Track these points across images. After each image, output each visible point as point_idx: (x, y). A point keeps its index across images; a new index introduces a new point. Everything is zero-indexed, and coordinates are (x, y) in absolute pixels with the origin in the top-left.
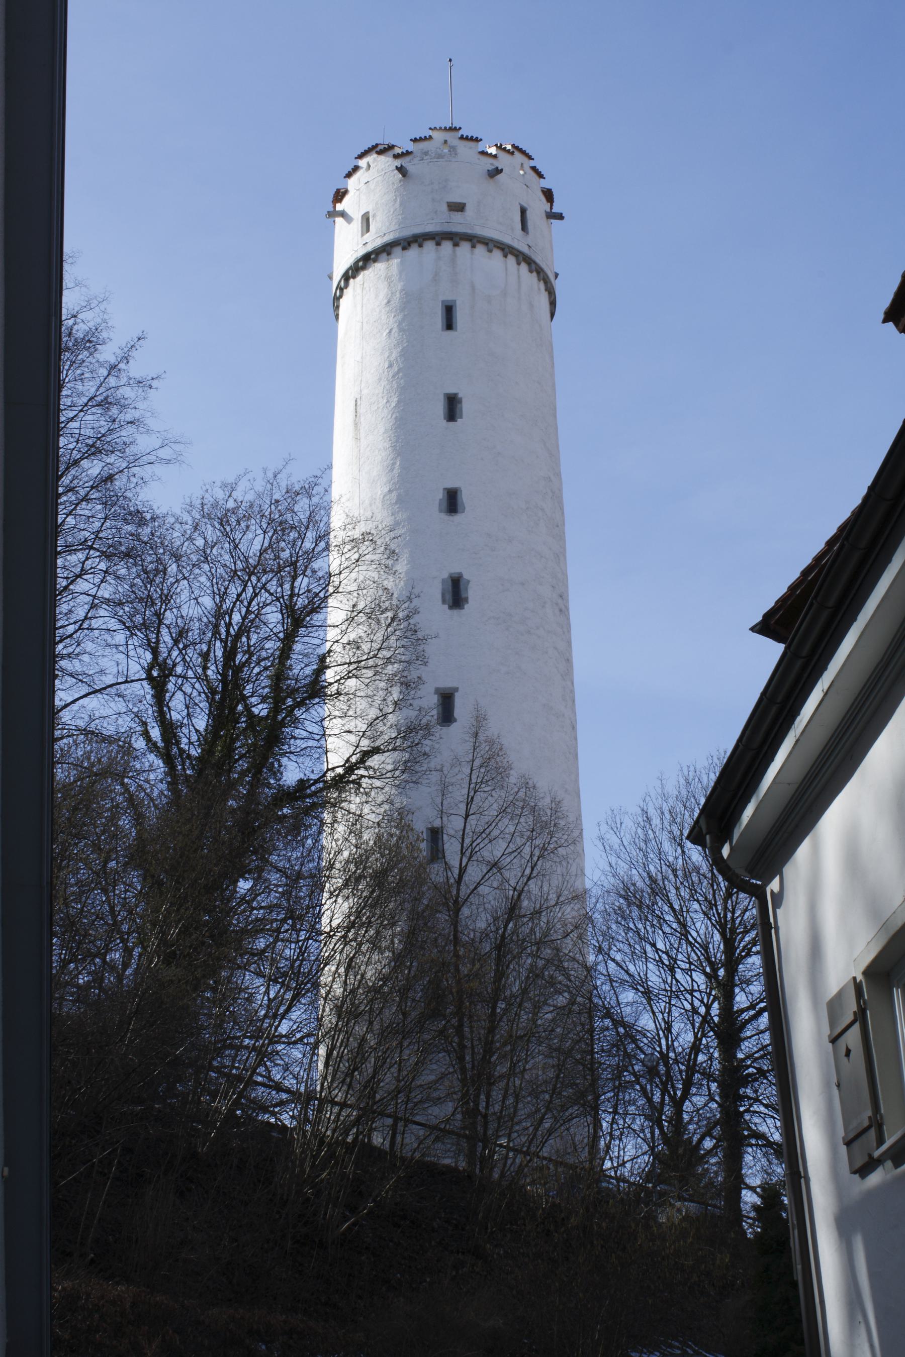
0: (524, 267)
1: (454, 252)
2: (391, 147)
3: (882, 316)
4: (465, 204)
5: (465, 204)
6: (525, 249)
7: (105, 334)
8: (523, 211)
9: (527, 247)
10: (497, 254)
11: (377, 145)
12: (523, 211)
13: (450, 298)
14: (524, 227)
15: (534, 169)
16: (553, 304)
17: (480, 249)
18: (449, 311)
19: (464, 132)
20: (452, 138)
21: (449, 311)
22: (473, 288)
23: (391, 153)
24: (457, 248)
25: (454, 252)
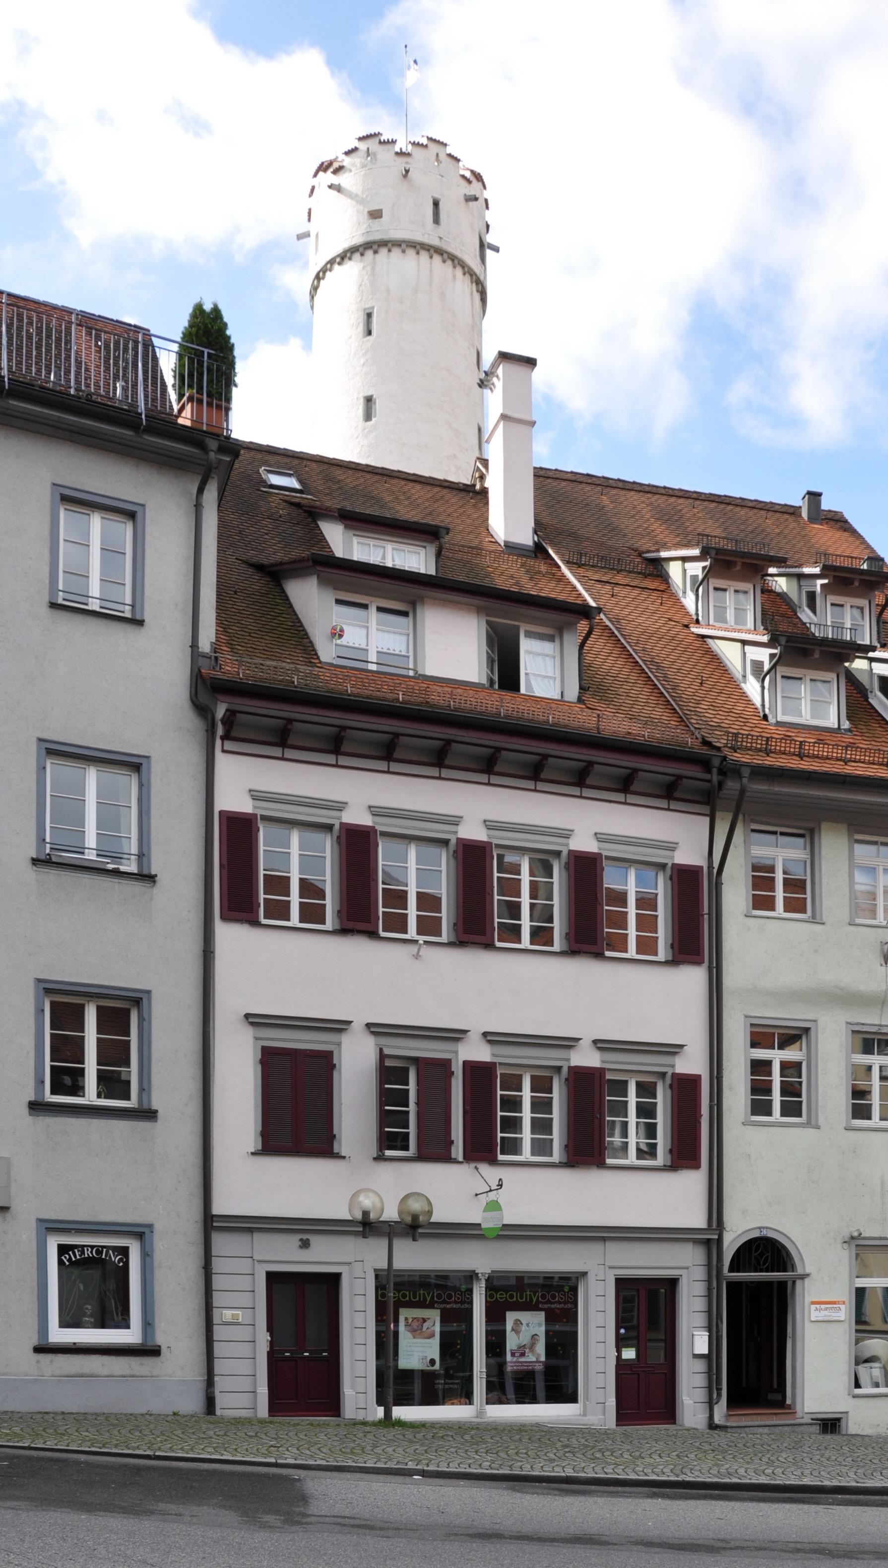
0: (437, 259)
1: (374, 259)
2: (330, 164)
3: (220, 307)
4: (381, 210)
5: (381, 210)
6: (435, 242)
7: (208, 307)
8: (436, 204)
9: (438, 240)
10: (411, 252)
11: (323, 163)
12: (436, 204)
13: (828, 1437)
14: (436, 220)
15: (450, 155)
16: (484, 300)
17: (396, 251)
18: (197, 126)
19: (384, 138)
20: (372, 144)
21: (197, 126)
22: (388, 291)
23: (331, 170)
24: (377, 256)
25: (374, 259)
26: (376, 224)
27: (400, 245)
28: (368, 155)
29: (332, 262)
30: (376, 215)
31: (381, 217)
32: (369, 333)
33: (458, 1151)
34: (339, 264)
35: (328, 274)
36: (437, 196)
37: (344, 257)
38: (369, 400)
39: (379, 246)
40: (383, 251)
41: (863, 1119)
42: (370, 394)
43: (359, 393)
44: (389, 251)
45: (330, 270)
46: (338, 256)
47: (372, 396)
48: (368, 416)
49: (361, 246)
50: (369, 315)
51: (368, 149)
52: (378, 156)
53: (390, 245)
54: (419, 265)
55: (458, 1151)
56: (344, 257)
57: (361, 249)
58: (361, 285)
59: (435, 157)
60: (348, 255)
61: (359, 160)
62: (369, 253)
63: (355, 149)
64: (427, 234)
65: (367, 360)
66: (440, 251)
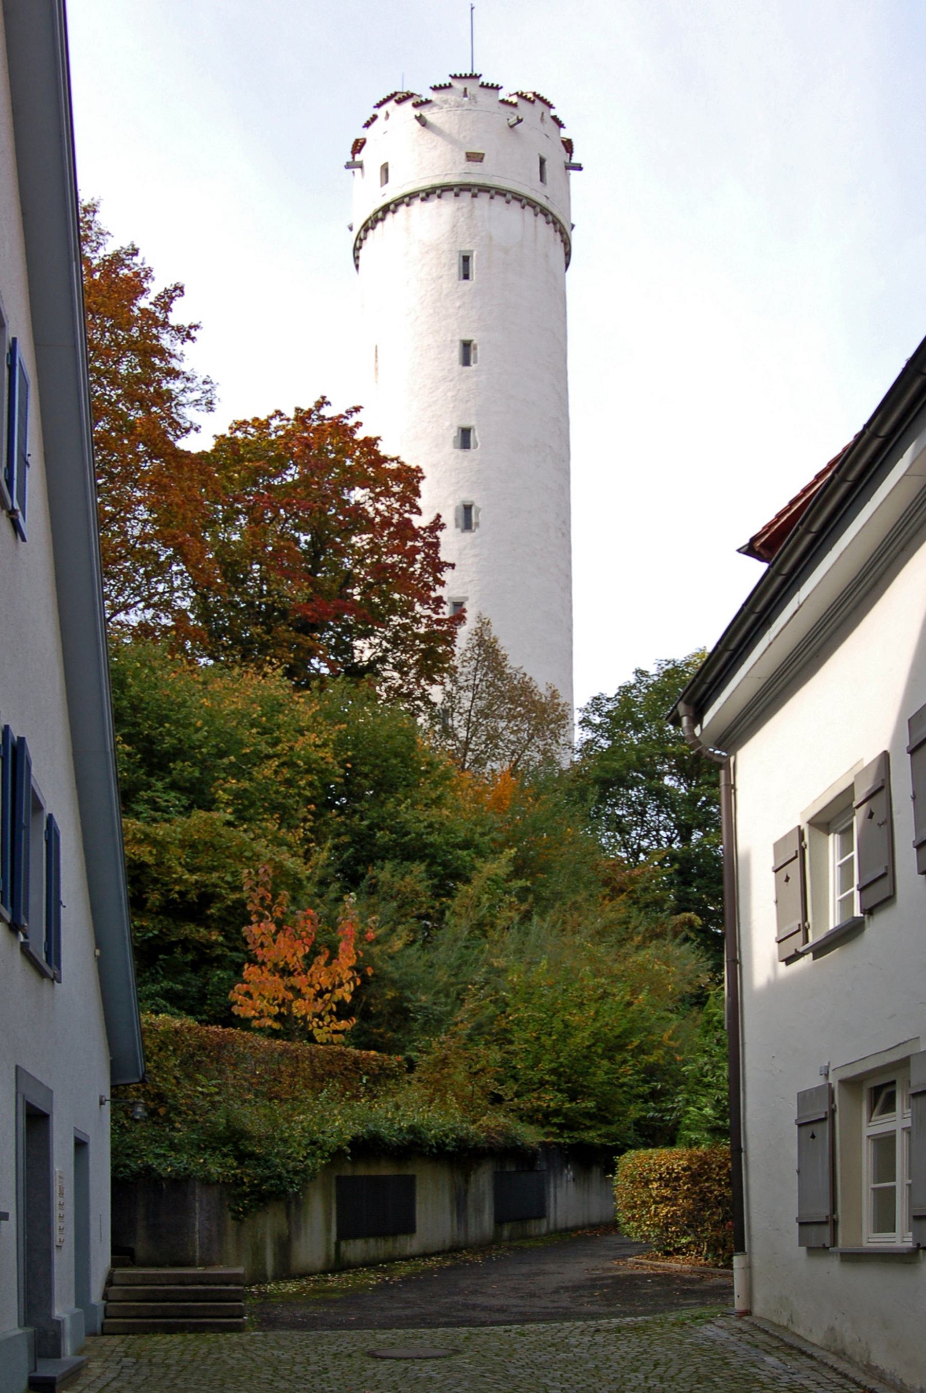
1: (472, 203)
6: (542, 201)
8: (542, 162)
10: (516, 205)
12: (542, 162)
15: (555, 118)
17: (499, 201)
19: (484, 80)
26: (475, 167)
27: (505, 195)
28: (465, 95)
29: (412, 196)
30: (474, 157)
31: (481, 160)
32: (466, 277)
33: (892, 1184)
34: (423, 200)
35: (390, 216)
36: (544, 156)
37: (428, 194)
38: (467, 346)
39: (480, 191)
40: (484, 197)
41: (894, 1141)
42: (468, 338)
43: (453, 335)
44: (492, 198)
45: (394, 212)
46: (423, 191)
47: (471, 341)
48: (466, 361)
49: (456, 186)
50: (466, 260)
51: (465, 89)
52: (479, 99)
53: (493, 192)
54: (523, 220)
55: (892, 1184)
56: (428, 194)
57: (456, 190)
58: (454, 226)
59: (540, 116)
60: (438, 192)
61: (453, 97)
62: (466, 196)
63: (375, 118)
64: (530, 188)
65: (464, 304)
66: (545, 212)
